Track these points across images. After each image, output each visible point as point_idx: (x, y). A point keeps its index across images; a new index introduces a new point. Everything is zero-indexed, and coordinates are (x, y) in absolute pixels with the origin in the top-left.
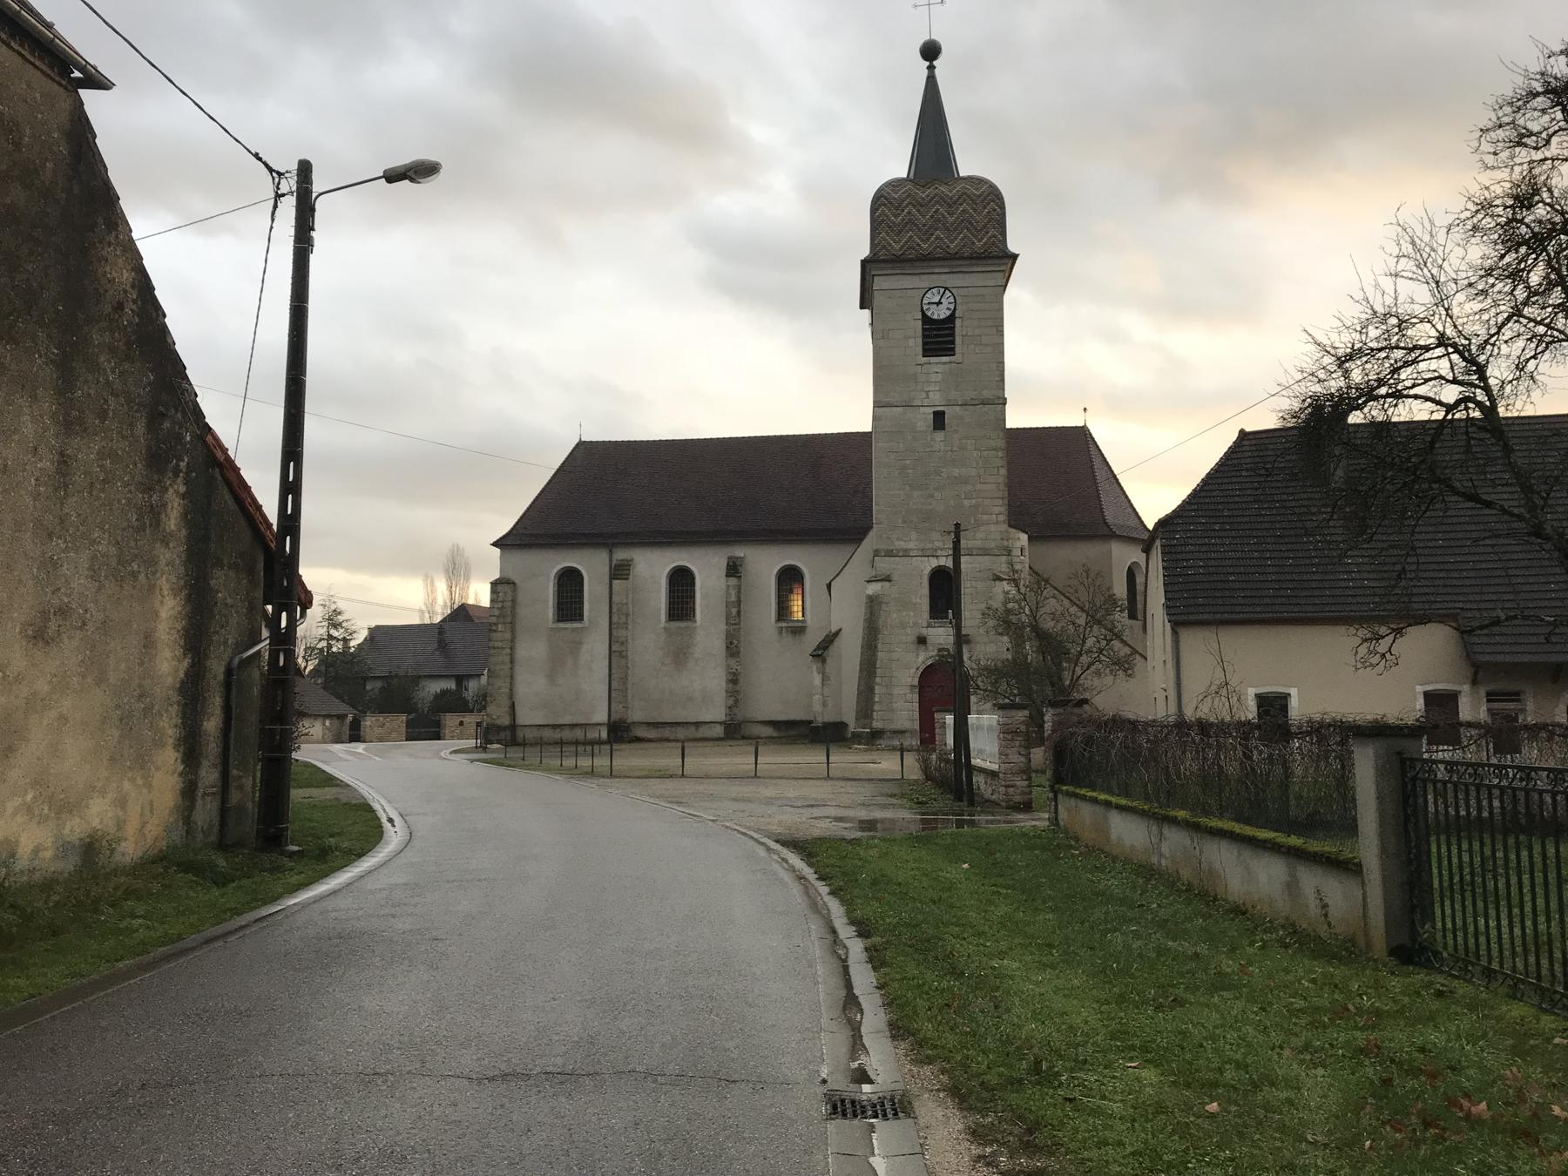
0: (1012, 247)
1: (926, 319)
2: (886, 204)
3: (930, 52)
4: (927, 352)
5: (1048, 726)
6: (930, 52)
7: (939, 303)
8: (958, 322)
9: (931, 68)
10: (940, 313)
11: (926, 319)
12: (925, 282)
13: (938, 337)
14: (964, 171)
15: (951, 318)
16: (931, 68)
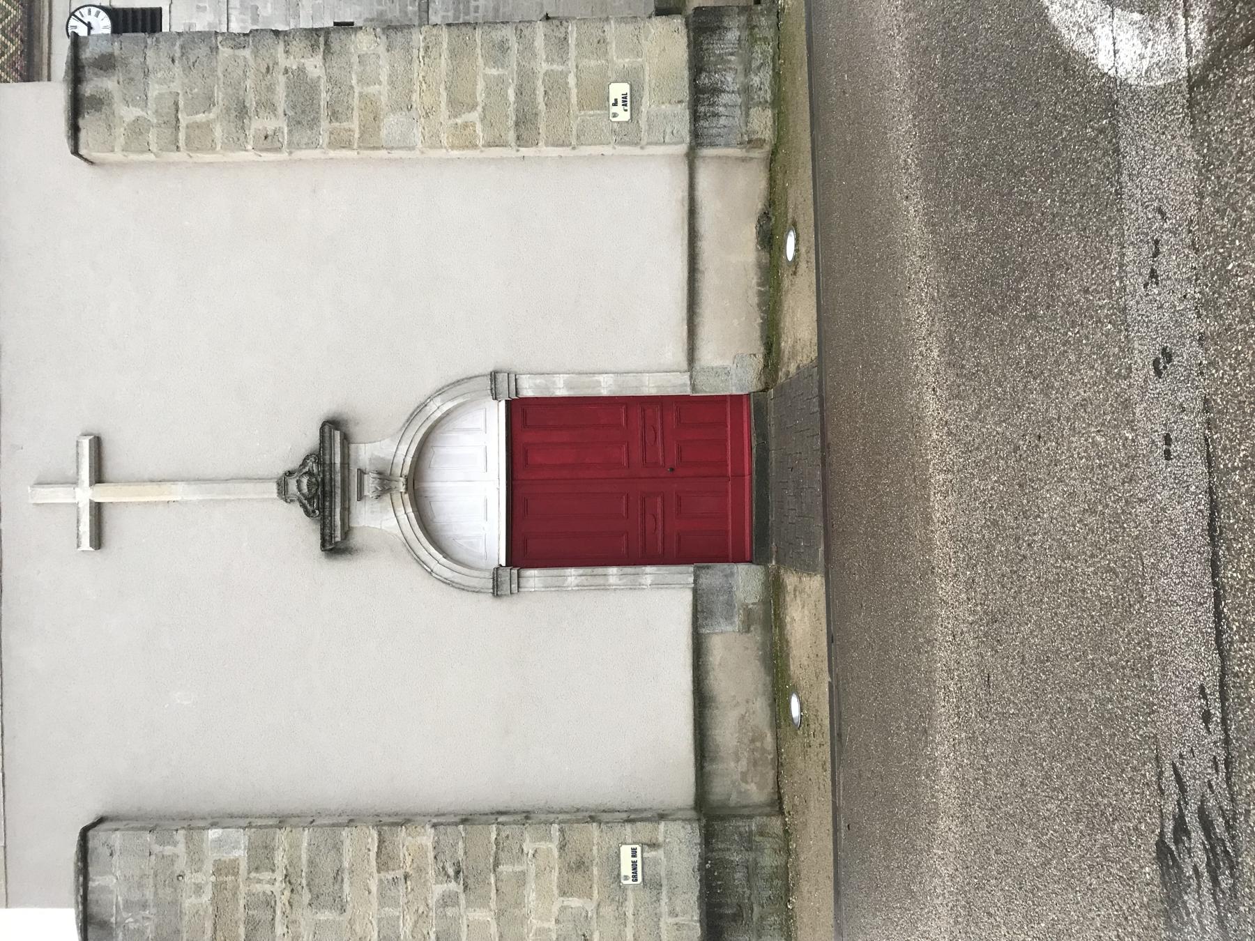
5: (626, 870)
7: (89, 26)
15: (112, 12)
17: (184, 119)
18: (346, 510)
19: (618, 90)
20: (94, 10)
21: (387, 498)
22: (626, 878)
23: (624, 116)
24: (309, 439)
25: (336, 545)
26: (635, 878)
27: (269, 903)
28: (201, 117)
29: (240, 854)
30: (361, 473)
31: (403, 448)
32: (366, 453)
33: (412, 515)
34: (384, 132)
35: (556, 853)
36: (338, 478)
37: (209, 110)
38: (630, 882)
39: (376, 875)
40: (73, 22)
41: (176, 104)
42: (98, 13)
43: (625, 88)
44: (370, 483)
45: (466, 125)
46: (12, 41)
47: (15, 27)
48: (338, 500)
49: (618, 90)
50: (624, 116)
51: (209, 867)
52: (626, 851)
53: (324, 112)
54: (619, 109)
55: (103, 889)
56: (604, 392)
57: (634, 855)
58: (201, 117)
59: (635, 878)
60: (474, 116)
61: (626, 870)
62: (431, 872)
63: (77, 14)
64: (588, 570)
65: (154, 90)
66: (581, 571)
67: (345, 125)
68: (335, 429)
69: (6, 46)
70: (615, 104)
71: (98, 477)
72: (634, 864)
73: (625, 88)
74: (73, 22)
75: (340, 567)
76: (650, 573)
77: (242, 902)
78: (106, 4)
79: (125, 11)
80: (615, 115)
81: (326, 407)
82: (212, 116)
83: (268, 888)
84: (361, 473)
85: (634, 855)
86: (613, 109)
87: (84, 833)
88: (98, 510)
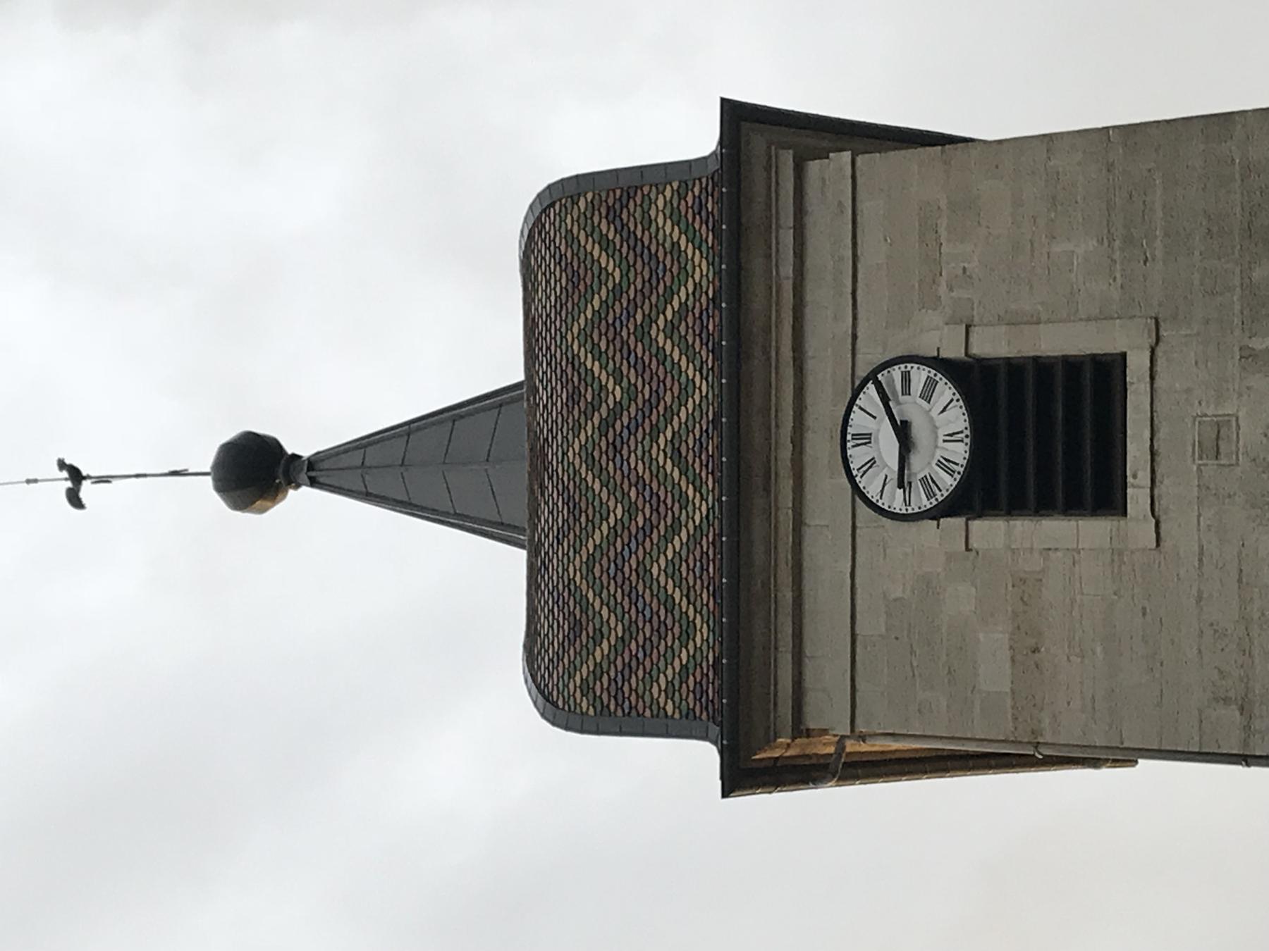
1: (977, 495)
3: (254, 470)
4: (1105, 496)
6: (254, 470)
8: (993, 344)
10: (945, 422)
11: (977, 495)
12: (826, 497)
13: (1047, 438)
14: (497, 359)
20: (920, 375)
24: (84, 501)
42: (906, 378)
78: (953, 350)
79: (1014, 368)
81: (56, 467)
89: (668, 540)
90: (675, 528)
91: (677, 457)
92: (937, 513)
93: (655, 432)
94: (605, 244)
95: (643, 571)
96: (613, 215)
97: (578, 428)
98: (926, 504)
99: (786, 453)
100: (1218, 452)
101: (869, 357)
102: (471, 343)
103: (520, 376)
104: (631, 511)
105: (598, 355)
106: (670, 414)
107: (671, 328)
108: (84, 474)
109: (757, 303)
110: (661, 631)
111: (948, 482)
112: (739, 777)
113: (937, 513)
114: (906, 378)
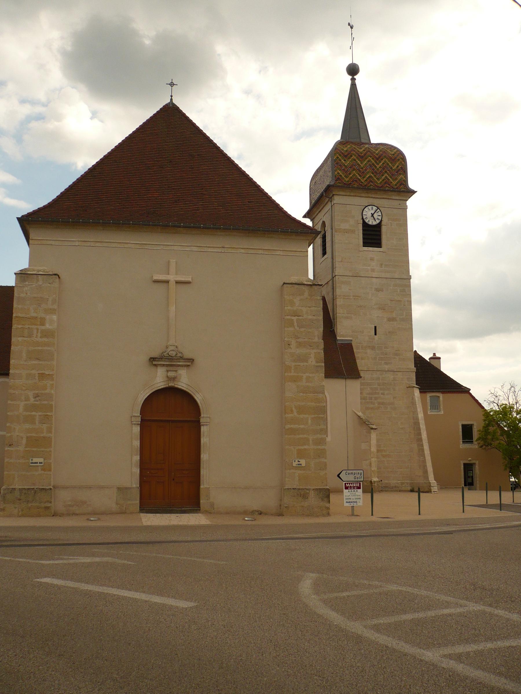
0: (411, 185)
1: (365, 225)
2: (339, 156)
3: (353, 70)
4: (366, 244)
6: (353, 70)
8: (384, 229)
9: (353, 80)
11: (365, 225)
12: (364, 201)
14: (375, 139)
16: (353, 80)
17: (295, 318)
18: (164, 365)
19: (303, 462)
20: (380, 218)
21: (166, 379)
22: (32, 460)
23: (294, 464)
25: (153, 361)
26: (32, 463)
27: (30, 336)
28: (296, 324)
29: (47, 326)
30: (176, 371)
31: (184, 386)
32: (183, 373)
33: (161, 388)
34: (290, 383)
35: (42, 435)
36: (174, 363)
37: (298, 326)
38: (31, 461)
39: (37, 372)
40: (375, 208)
41: (300, 316)
42: (380, 216)
43: (304, 465)
44: (171, 374)
45: (292, 411)
46: (366, 180)
47: (372, 182)
48: (167, 363)
49: (303, 462)
50: (294, 464)
51: (43, 315)
52: (41, 460)
53: (296, 364)
54: (297, 463)
55: (38, 281)
56: (202, 456)
57: (40, 463)
58: (296, 324)
59: (32, 463)
60: (295, 414)
61: (35, 460)
62: (37, 392)
63: (378, 210)
64: (202, 436)
65: (304, 309)
66: (139, 446)
67: (293, 371)
68: (192, 360)
69: (364, 178)
70: (298, 461)
71: (177, 282)
72: (37, 463)
73: (304, 465)
74: (375, 208)
75: (145, 358)
76: (137, 471)
77: (30, 326)
78: (383, 223)
79: (380, 231)
80: (295, 461)
82: (296, 327)
83: (35, 335)
84: (176, 371)
85: (40, 463)
86: (297, 461)
87: (58, 275)
88: (167, 282)
89: (359, 174)
90: (360, 176)
91: (370, 177)
92: (364, 222)
93: (373, 173)
94: (398, 166)
95: (354, 169)
96: (401, 168)
97: (373, 159)
98: (364, 218)
99: (370, 195)
100: (399, 301)
101: (380, 208)
102: (377, 134)
103: (372, 142)
104: (362, 168)
105: (383, 164)
106: (375, 176)
107: (386, 177)
108: (169, 101)
109: (390, 193)
110: (346, 172)
111: (367, 221)
112: (470, 390)
113: (363, 218)
114: (380, 216)
